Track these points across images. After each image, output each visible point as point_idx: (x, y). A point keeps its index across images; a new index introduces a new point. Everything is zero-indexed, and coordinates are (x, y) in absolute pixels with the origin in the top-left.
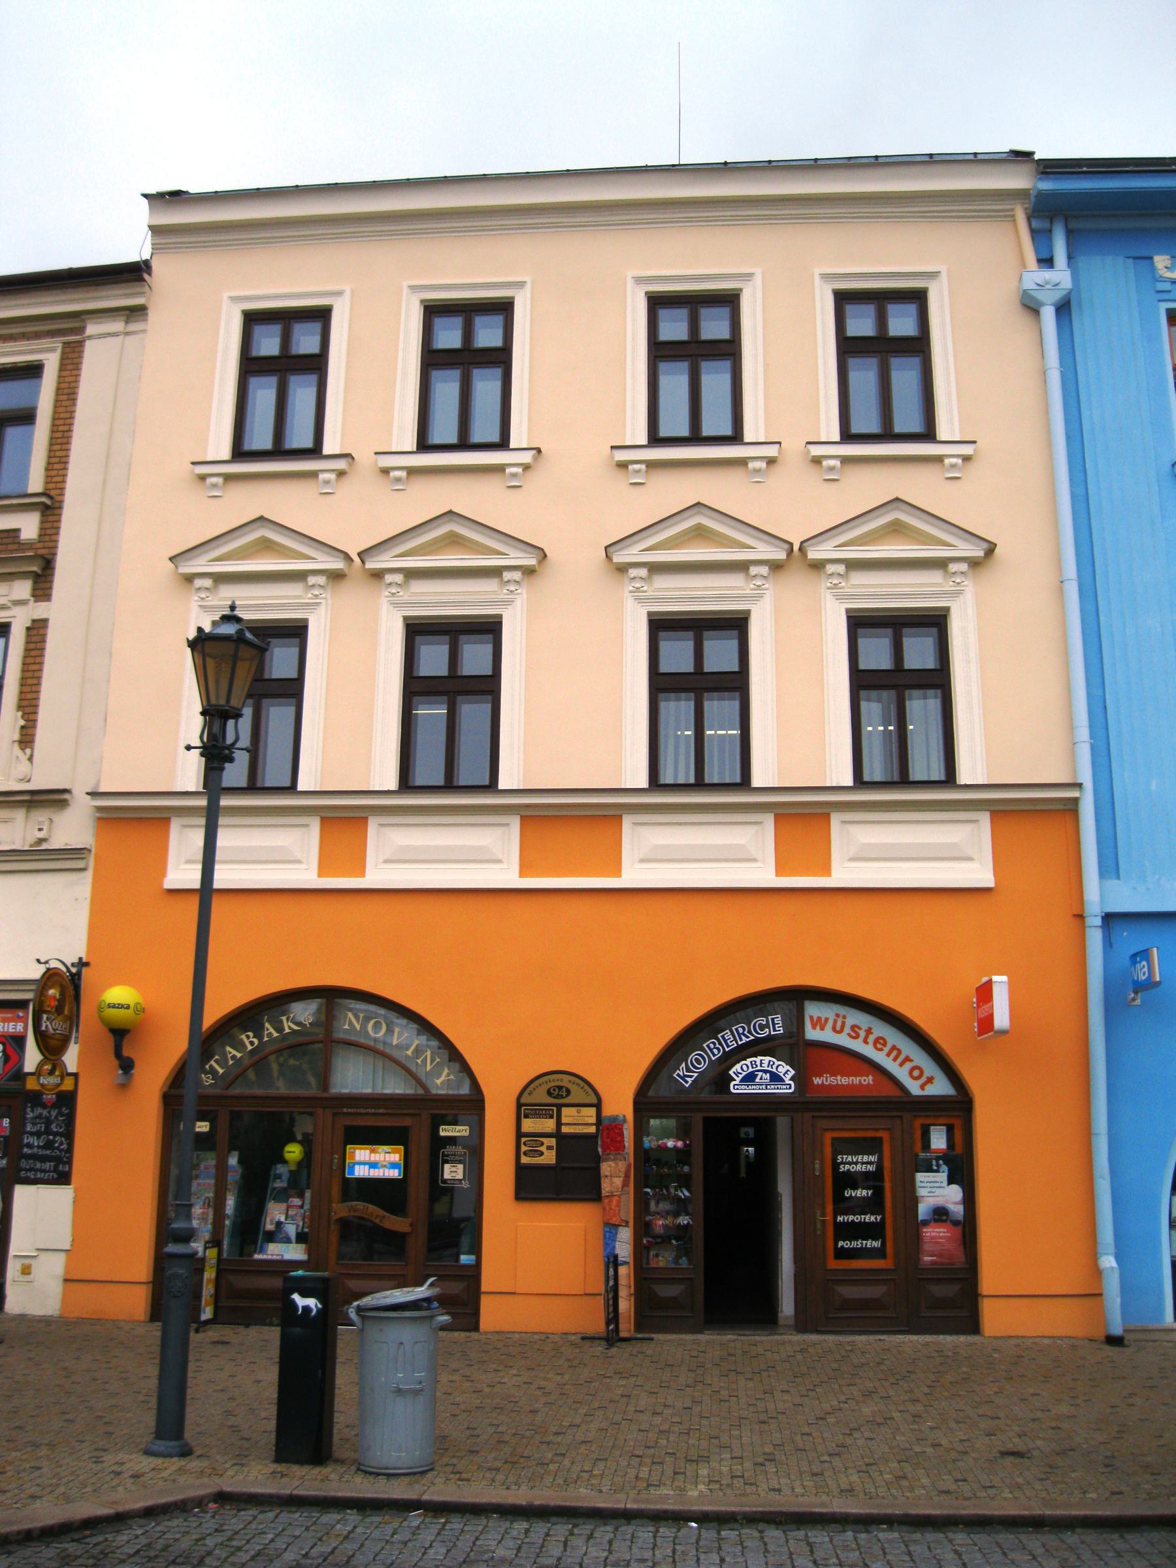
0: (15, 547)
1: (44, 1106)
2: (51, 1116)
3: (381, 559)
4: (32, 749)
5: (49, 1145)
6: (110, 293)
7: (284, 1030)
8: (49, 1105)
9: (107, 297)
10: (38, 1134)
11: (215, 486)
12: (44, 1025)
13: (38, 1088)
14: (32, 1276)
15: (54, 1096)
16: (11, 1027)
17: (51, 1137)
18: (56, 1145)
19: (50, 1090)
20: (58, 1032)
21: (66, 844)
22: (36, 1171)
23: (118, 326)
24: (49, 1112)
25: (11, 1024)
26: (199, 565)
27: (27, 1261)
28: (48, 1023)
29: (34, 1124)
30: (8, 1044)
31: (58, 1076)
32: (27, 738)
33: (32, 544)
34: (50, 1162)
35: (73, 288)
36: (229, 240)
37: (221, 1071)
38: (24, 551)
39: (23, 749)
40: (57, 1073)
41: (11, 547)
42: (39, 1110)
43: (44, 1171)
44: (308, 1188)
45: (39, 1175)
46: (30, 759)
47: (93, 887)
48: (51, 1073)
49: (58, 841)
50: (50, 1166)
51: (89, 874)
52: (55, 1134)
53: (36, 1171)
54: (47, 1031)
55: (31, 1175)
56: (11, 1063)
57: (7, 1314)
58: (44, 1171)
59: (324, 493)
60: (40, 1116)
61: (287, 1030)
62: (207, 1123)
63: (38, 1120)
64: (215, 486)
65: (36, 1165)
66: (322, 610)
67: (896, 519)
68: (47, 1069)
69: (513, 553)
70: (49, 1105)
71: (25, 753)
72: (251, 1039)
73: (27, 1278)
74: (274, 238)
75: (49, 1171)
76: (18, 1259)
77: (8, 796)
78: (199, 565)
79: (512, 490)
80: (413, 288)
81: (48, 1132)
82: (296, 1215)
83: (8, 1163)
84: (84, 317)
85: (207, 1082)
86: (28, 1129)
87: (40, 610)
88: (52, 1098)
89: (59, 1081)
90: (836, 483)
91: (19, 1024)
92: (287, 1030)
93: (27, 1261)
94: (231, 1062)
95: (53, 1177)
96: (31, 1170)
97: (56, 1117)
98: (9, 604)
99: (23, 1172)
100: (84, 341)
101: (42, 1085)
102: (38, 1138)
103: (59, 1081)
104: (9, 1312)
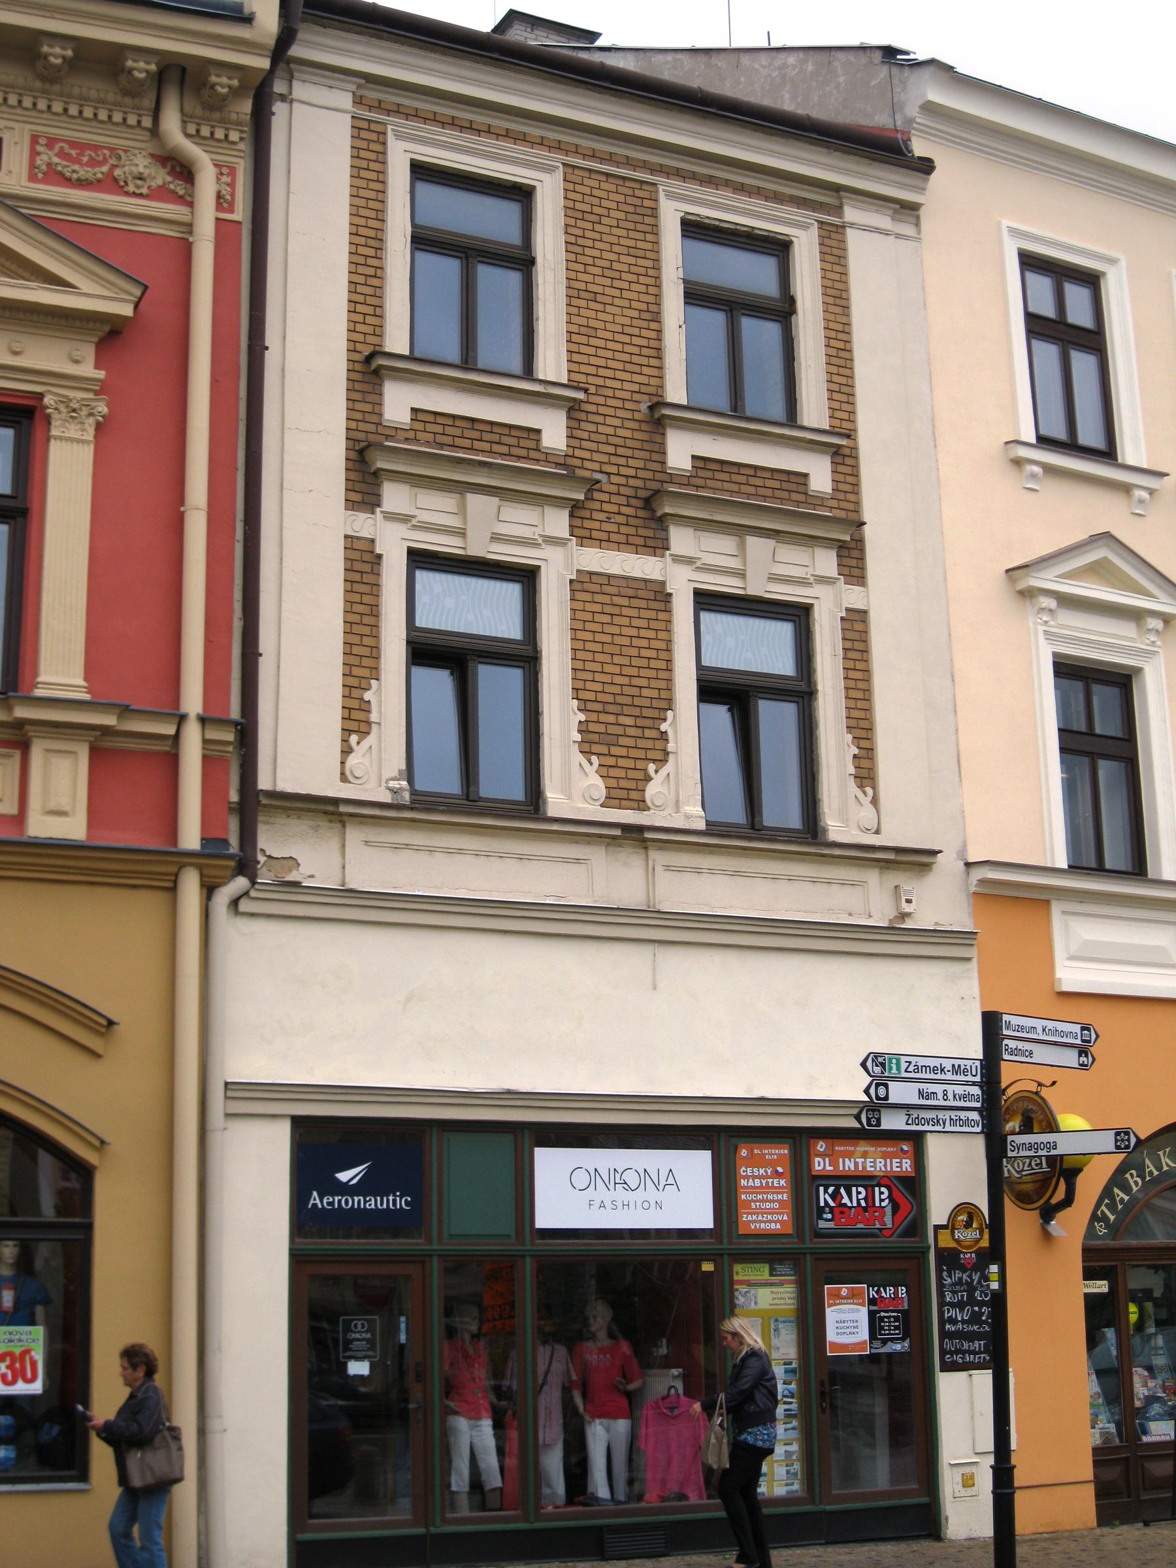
0: (801, 498)
1: (963, 1269)
2: (972, 1281)
3: (1044, 577)
4: (874, 788)
5: (975, 1319)
6: (880, 174)
7: (1163, 1168)
8: (969, 1266)
9: (878, 180)
10: (960, 1305)
11: (1033, 476)
12: (1005, 1170)
13: (953, 1245)
14: (975, 1488)
15: (973, 1255)
16: (895, 1165)
17: (976, 1309)
18: (984, 1318)
19: (968, 1247)
20: (1024, 1173)
21: (936, 924)
22: (964, 1352)
23: (883, 220)
24: (970, 1276)
25: (895, 1161)
26: (1046, 580)
27: (967, 1470)
28: (1009, 1166)
29: (954, 1292)
30: (893, 1187)
31: (977, 1228)
32: (864, 773)
33: (822, 498)
34: (979, 1340)
35: (844, 152)
36: (1101, 182)
37: (1112, 1218)
38: (815, 506)
39: (861, 787)
40: (974, 1225)
41: (794, 496)
42: (958, 1274)
43: (973, 1352)
44: (401, 1314)
45: (969, 1358)
46: (875, 801)
47: (981, 985)
48: (968, 1225)
49: (925, 917)
50: (980, 1344)
51: (974, 964)
52: (982, 1304)
53: (964, 1352)
54: (1010, 1177)
55: (958, 1358)
56: (902, 1213)
57: (951, 1540)
58: (973, 1352)
59: (1027, 488)
60: (960, 1282)
61: (1165, 1168)
62: (1105, 1282)
63: (958, 1288)
64: (1033, 476)
65: (963, 1346)
66: (1160, 660)
67: (1105, 557)
68: (963, 1221)
69: (1163, 597)
70: (969, 1266)
71: (865, 793)
72: (1135, 1179)
73: (970, 1491)
74: (1045, 165)
75: (980, 1352)
76: (955, 1470)
77: (867, 852)
78: (1046, 580)
79: (1136, 518)
80: (1013, 232)
81: (972, 1301)
82: (1155, 1387)
83: (911, 1346)
84: (842, 194)
85: (1101, 1231)
86: (948, 1300)
87: (853, 597)
88: (971, 1258)
89: (978, 1236)
90: (1035, 493)
91: (904, 1161)
92: (1165, 1168)
93: (967, 1470)
94: (1120, 1207)
95: (984, 1357)
96: (957, 1352)
97: (979, 1282)
98: (812, 580)
99: (948, 1356)
100: (844, 227)
101: (958, 1241)
102: (962, 1310)
103: (978, 1236)
104: (953, 1538)
